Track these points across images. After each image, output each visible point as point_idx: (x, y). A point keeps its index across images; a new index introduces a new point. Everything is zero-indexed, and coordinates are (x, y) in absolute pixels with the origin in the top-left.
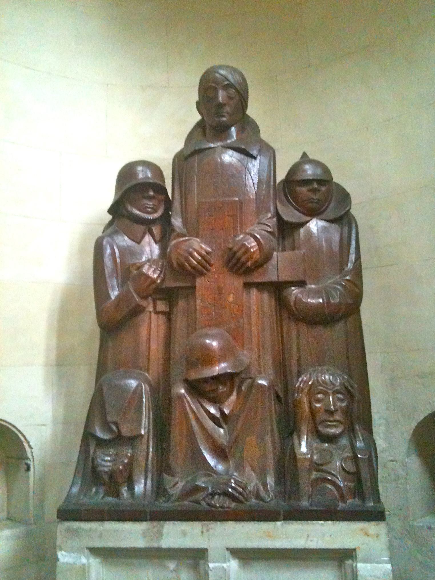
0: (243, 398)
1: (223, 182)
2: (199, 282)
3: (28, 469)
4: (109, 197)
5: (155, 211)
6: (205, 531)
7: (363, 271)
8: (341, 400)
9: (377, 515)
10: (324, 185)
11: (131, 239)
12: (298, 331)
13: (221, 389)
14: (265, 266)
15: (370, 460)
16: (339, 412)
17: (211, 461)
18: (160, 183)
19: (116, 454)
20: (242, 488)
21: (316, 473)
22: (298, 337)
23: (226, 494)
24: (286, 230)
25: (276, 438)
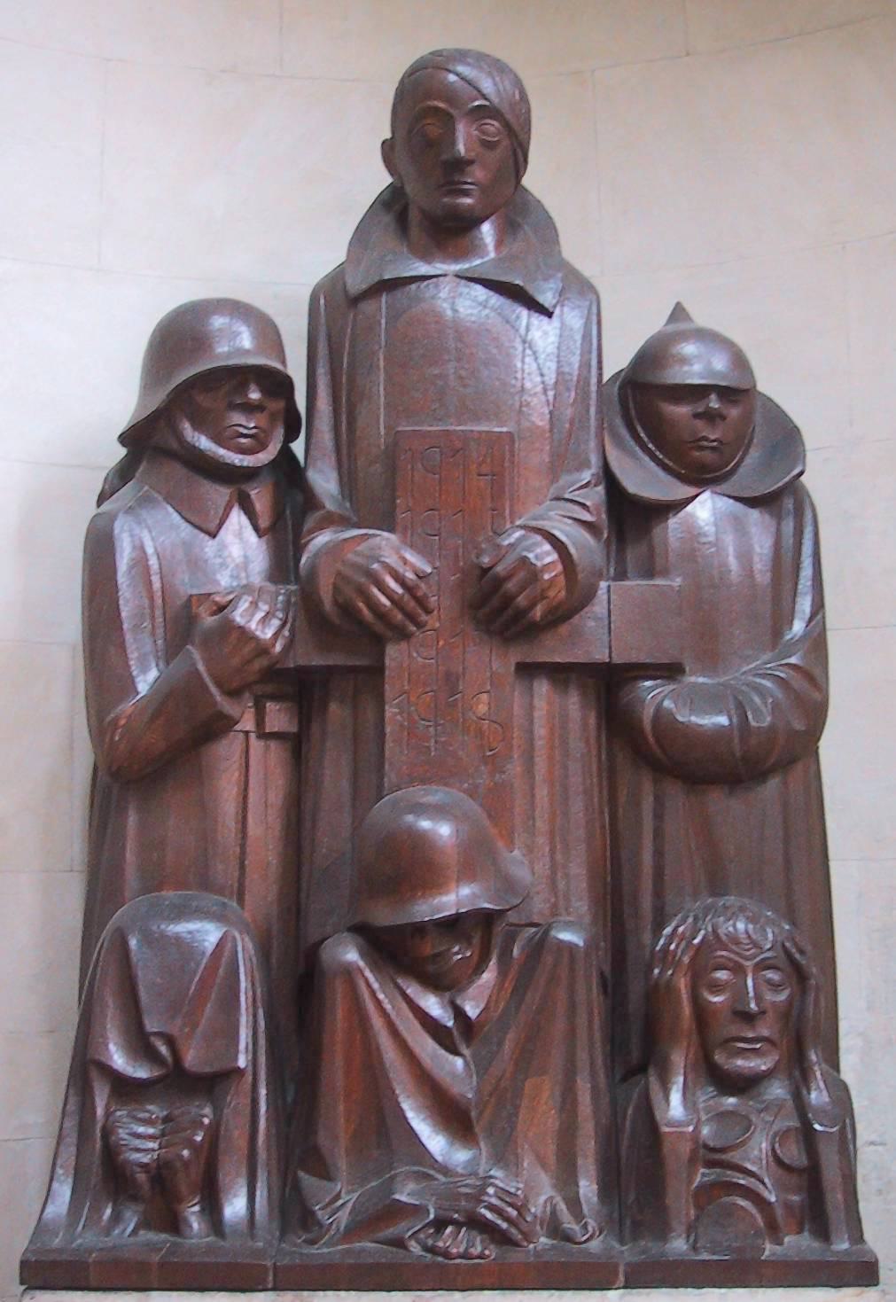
0: (520, 981)
1: (461, 378)
2: (394, 654)
4: (119, 397)
5: (260, 444)
8: (776, 987)
10: (735, 402)
11: (188, 521)
13: (459, 953)
15: (842, 1131)
16: (770, 1014)
17: (435, 1142)
19: (166, 1120)
20: (517, 1210)
21: (707, 1171)
22: (659, 816)
23: (476, 1223)
24: (629, 519)
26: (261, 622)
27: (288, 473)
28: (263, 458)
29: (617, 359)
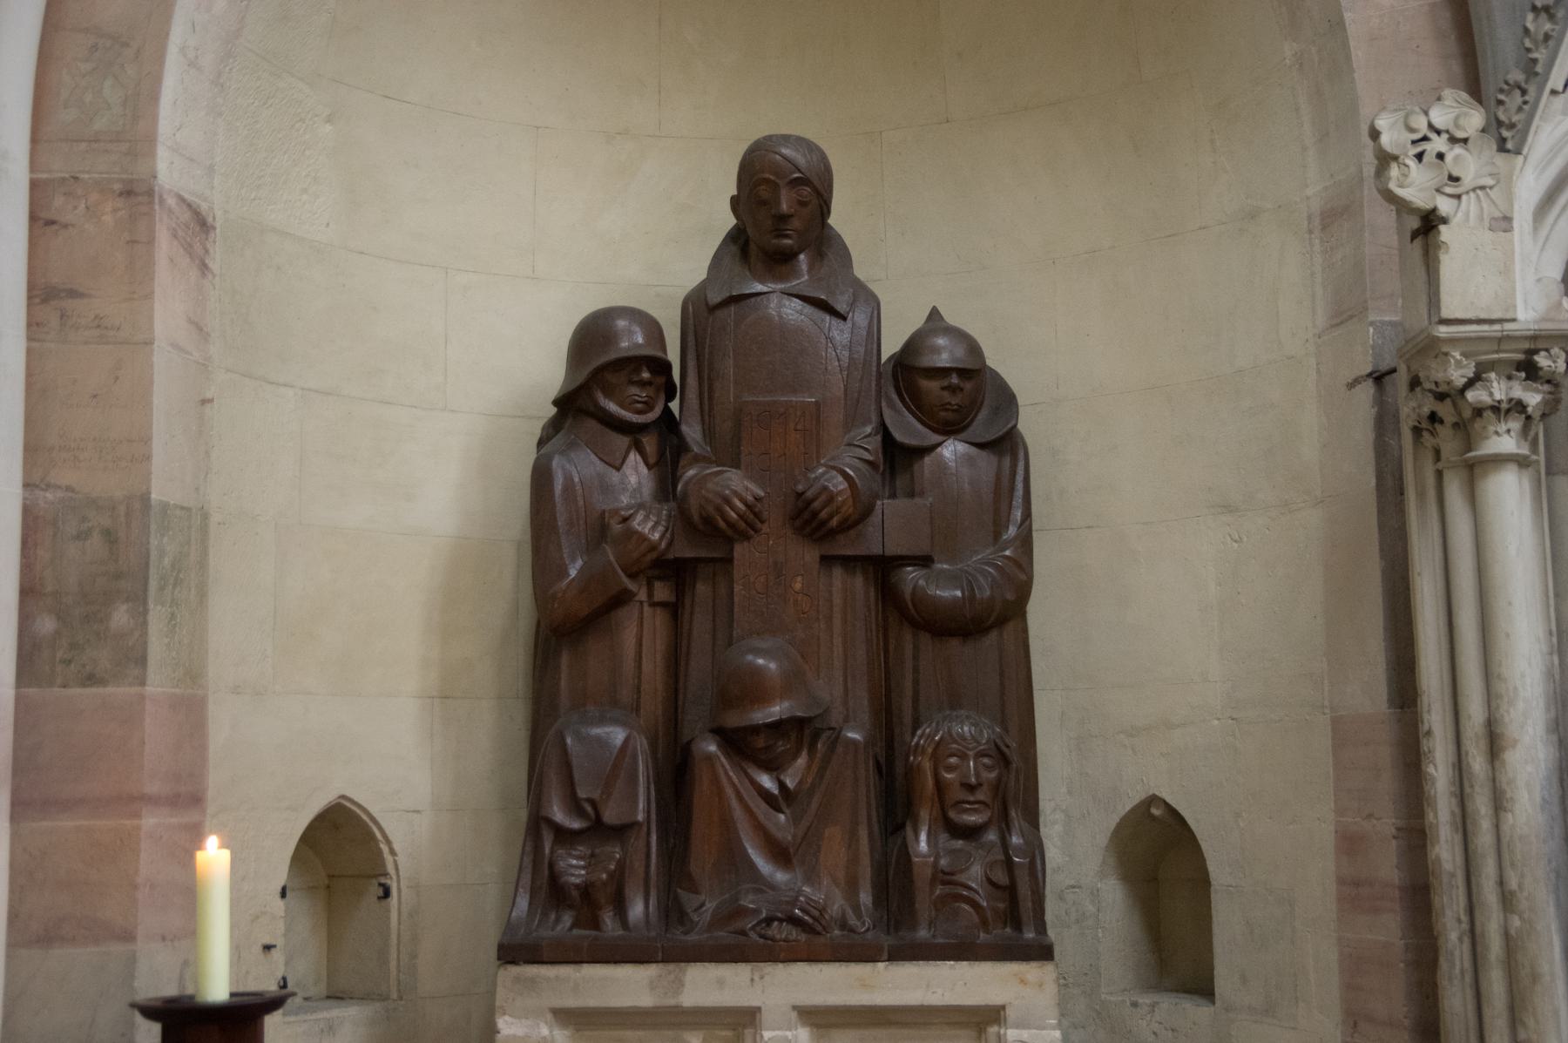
2: (739, 550)
3: (387, 893)
4: (545, 370)
5: (649, 406)
6: (756, 978)
7: (1034, 534)
8: (989, 768)
9: (1043, 952)
10: (969, 379)
12: (916, 648)
13: (781, 746)
14: (860, 527)
15: (1032, 863)
16: (985, 787)
18: (660, 354)
19: (593, 855)
22: (916, 658)
24: (897, 459)
25: (876, 828)
26: (650, 528)
27: (669, 423)
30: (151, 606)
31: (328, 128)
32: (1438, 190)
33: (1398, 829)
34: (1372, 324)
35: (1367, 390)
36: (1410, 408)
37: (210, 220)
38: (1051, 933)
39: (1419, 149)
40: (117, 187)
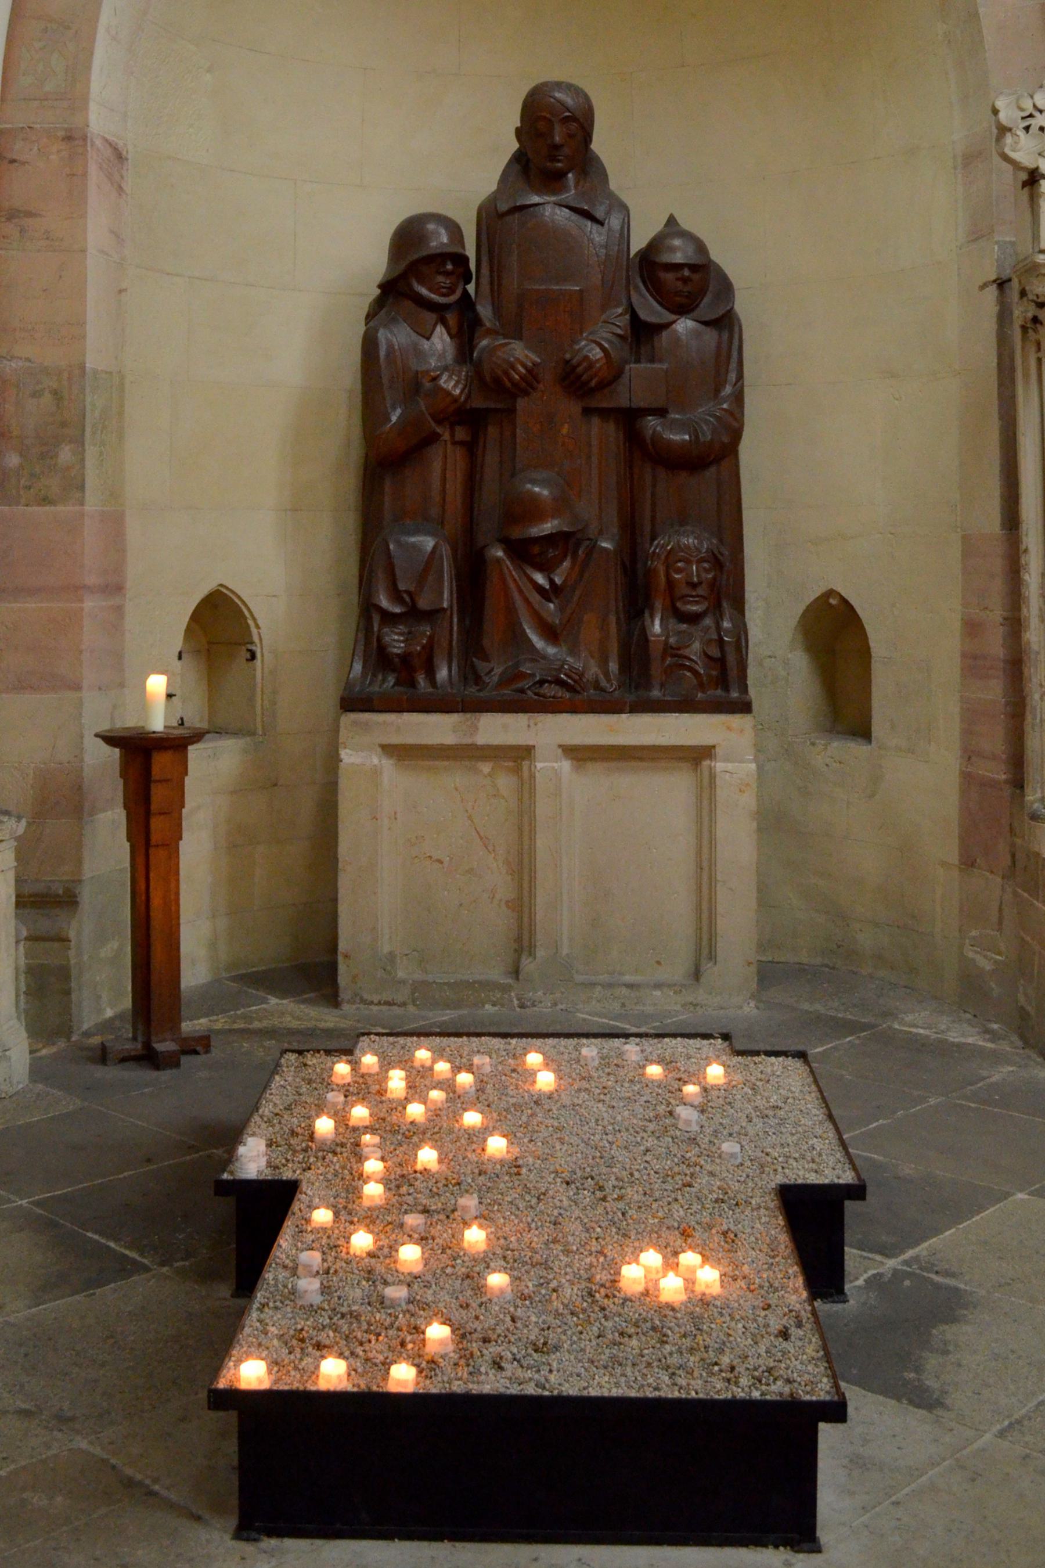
2: (521, 403)
3: (253, 657)
4: (371, 261)
5: (452, 291)
6: (532, 725)
7: (746, 389)
8: (707, 571)
9: (744, 707)
13: (551, 553)
16: (704, 585)
18: (460, 251)
19: (410, 633)
22: (654, 486)
23: (560, 683)
24: (642, 334)
27: (466, 303)
28: (452, 298)
29: (638, 242)
30: (87, 447)
31: (208, 77)
32: (1040, 154)
33: (1005, 619)
34: (997, 243)
35: (992, 292)
36: (1021, 312)
37: (124, 153)
38: (752, 691)
39: (1026, 124)
40: (61, 134)
